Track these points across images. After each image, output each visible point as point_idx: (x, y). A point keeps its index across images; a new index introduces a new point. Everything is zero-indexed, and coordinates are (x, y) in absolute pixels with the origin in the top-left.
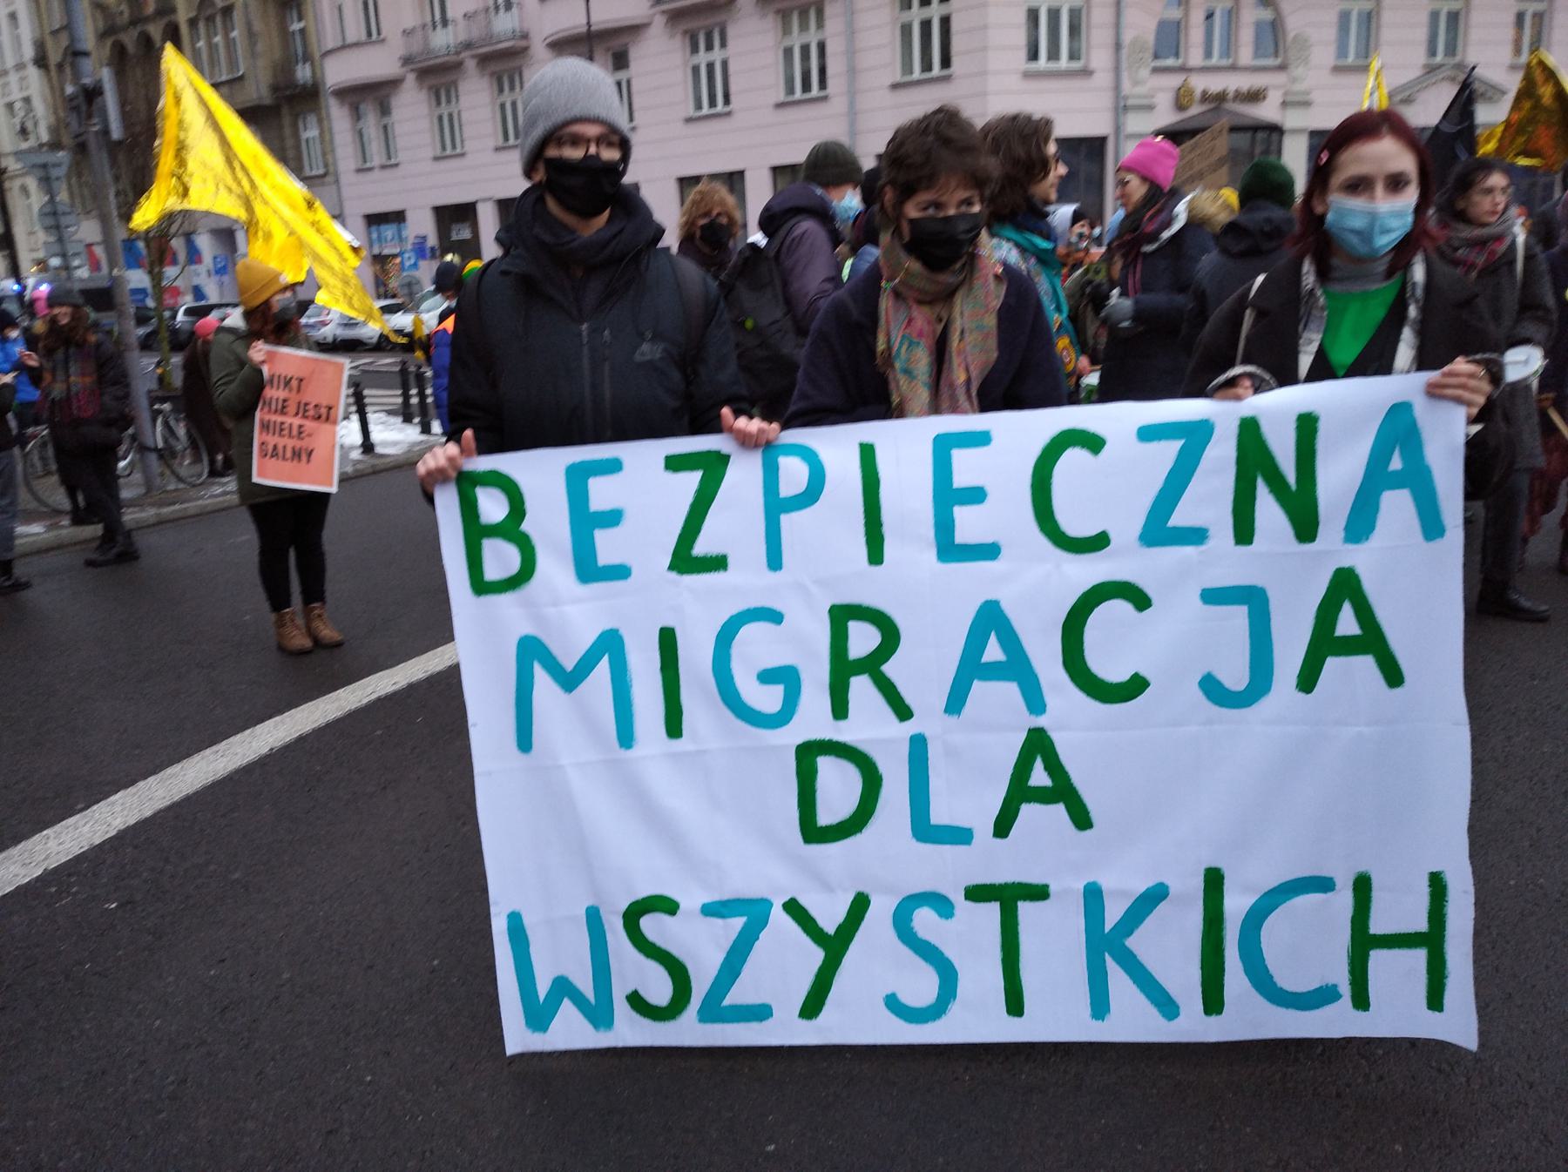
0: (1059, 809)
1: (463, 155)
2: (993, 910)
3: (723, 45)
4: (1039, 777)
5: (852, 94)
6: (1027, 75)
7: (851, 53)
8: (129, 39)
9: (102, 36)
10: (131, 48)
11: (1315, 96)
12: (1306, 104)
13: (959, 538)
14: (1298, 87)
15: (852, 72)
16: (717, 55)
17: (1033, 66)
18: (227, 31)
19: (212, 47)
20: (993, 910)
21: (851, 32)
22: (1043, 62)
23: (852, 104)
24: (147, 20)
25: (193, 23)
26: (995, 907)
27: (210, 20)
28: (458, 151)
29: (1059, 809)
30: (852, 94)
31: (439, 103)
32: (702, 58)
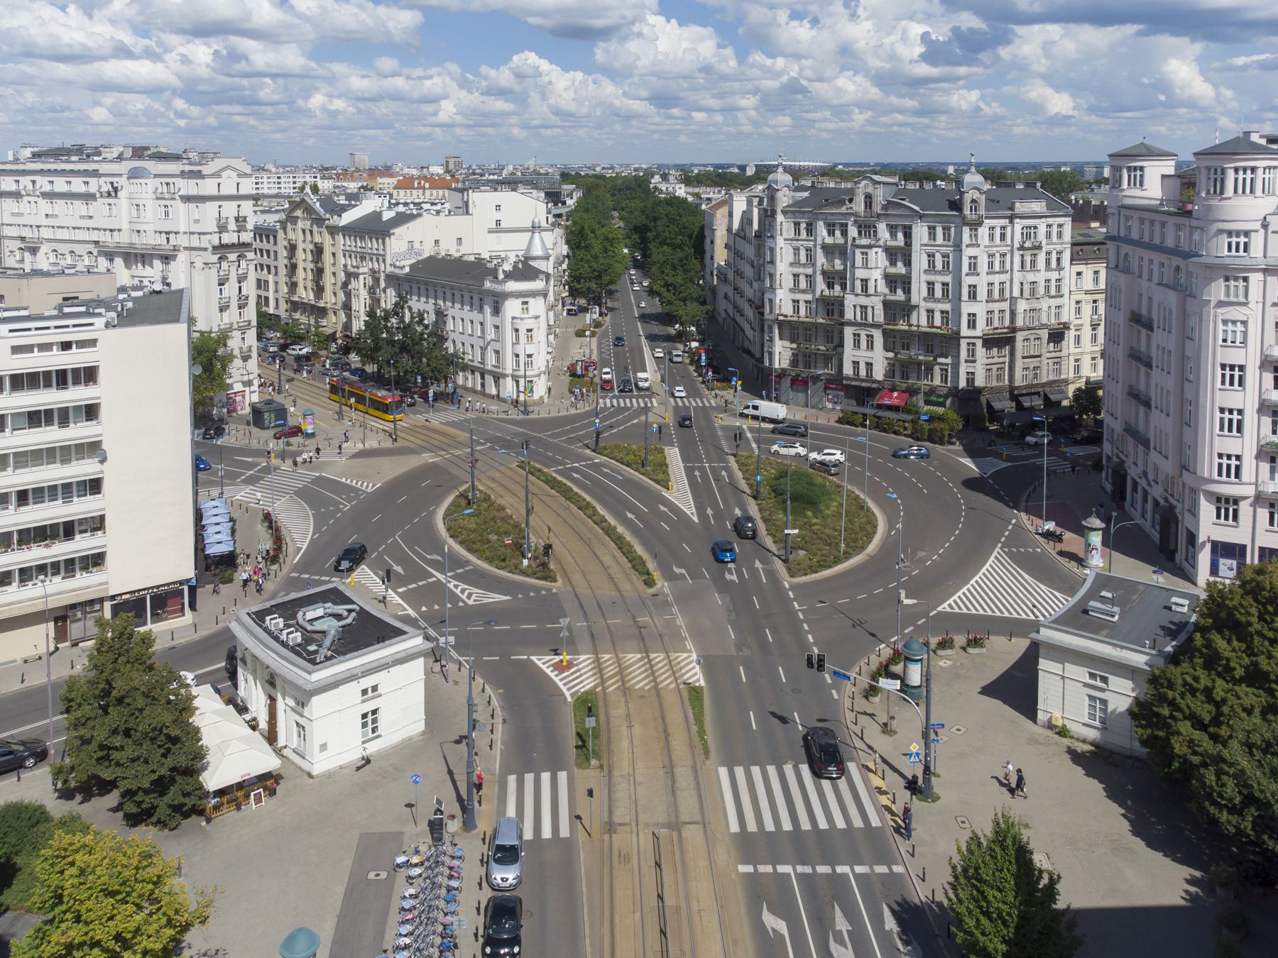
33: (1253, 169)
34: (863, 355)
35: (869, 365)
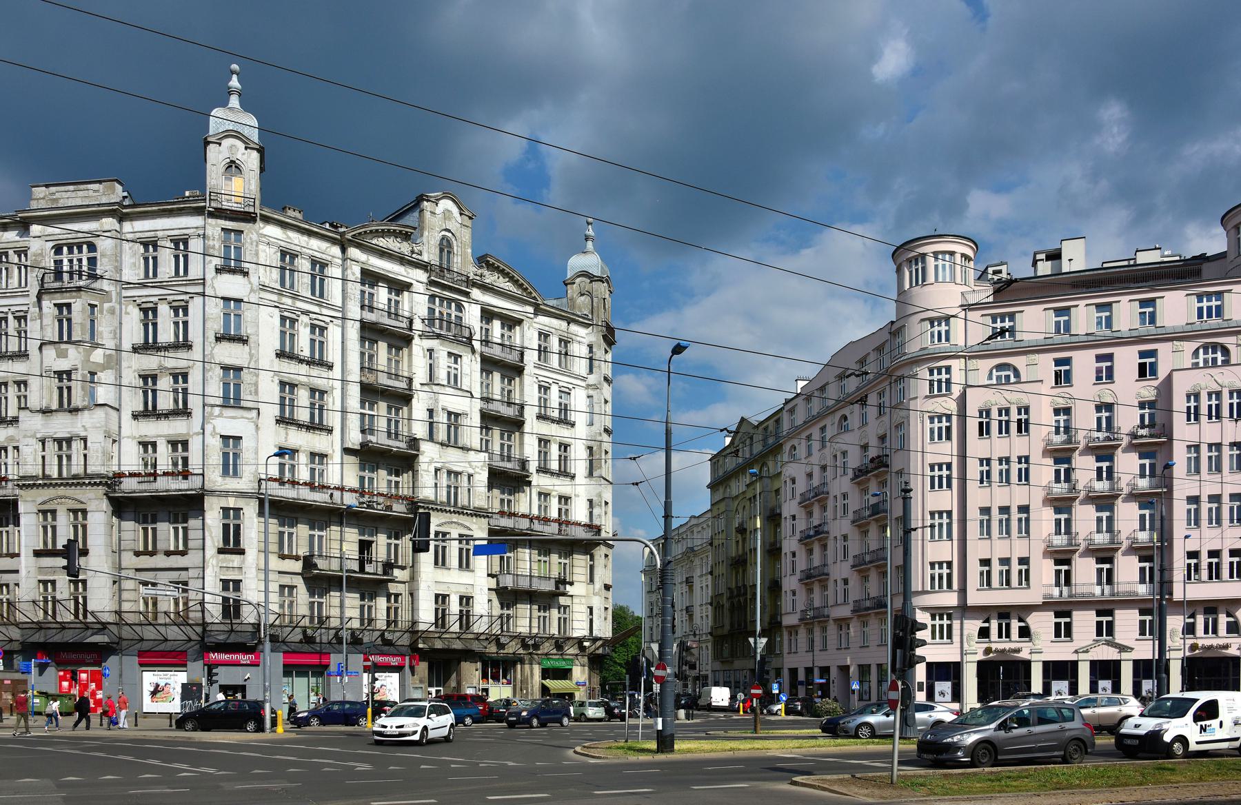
33: (924, 256)
34: (454, 580)
35: (466, 600)
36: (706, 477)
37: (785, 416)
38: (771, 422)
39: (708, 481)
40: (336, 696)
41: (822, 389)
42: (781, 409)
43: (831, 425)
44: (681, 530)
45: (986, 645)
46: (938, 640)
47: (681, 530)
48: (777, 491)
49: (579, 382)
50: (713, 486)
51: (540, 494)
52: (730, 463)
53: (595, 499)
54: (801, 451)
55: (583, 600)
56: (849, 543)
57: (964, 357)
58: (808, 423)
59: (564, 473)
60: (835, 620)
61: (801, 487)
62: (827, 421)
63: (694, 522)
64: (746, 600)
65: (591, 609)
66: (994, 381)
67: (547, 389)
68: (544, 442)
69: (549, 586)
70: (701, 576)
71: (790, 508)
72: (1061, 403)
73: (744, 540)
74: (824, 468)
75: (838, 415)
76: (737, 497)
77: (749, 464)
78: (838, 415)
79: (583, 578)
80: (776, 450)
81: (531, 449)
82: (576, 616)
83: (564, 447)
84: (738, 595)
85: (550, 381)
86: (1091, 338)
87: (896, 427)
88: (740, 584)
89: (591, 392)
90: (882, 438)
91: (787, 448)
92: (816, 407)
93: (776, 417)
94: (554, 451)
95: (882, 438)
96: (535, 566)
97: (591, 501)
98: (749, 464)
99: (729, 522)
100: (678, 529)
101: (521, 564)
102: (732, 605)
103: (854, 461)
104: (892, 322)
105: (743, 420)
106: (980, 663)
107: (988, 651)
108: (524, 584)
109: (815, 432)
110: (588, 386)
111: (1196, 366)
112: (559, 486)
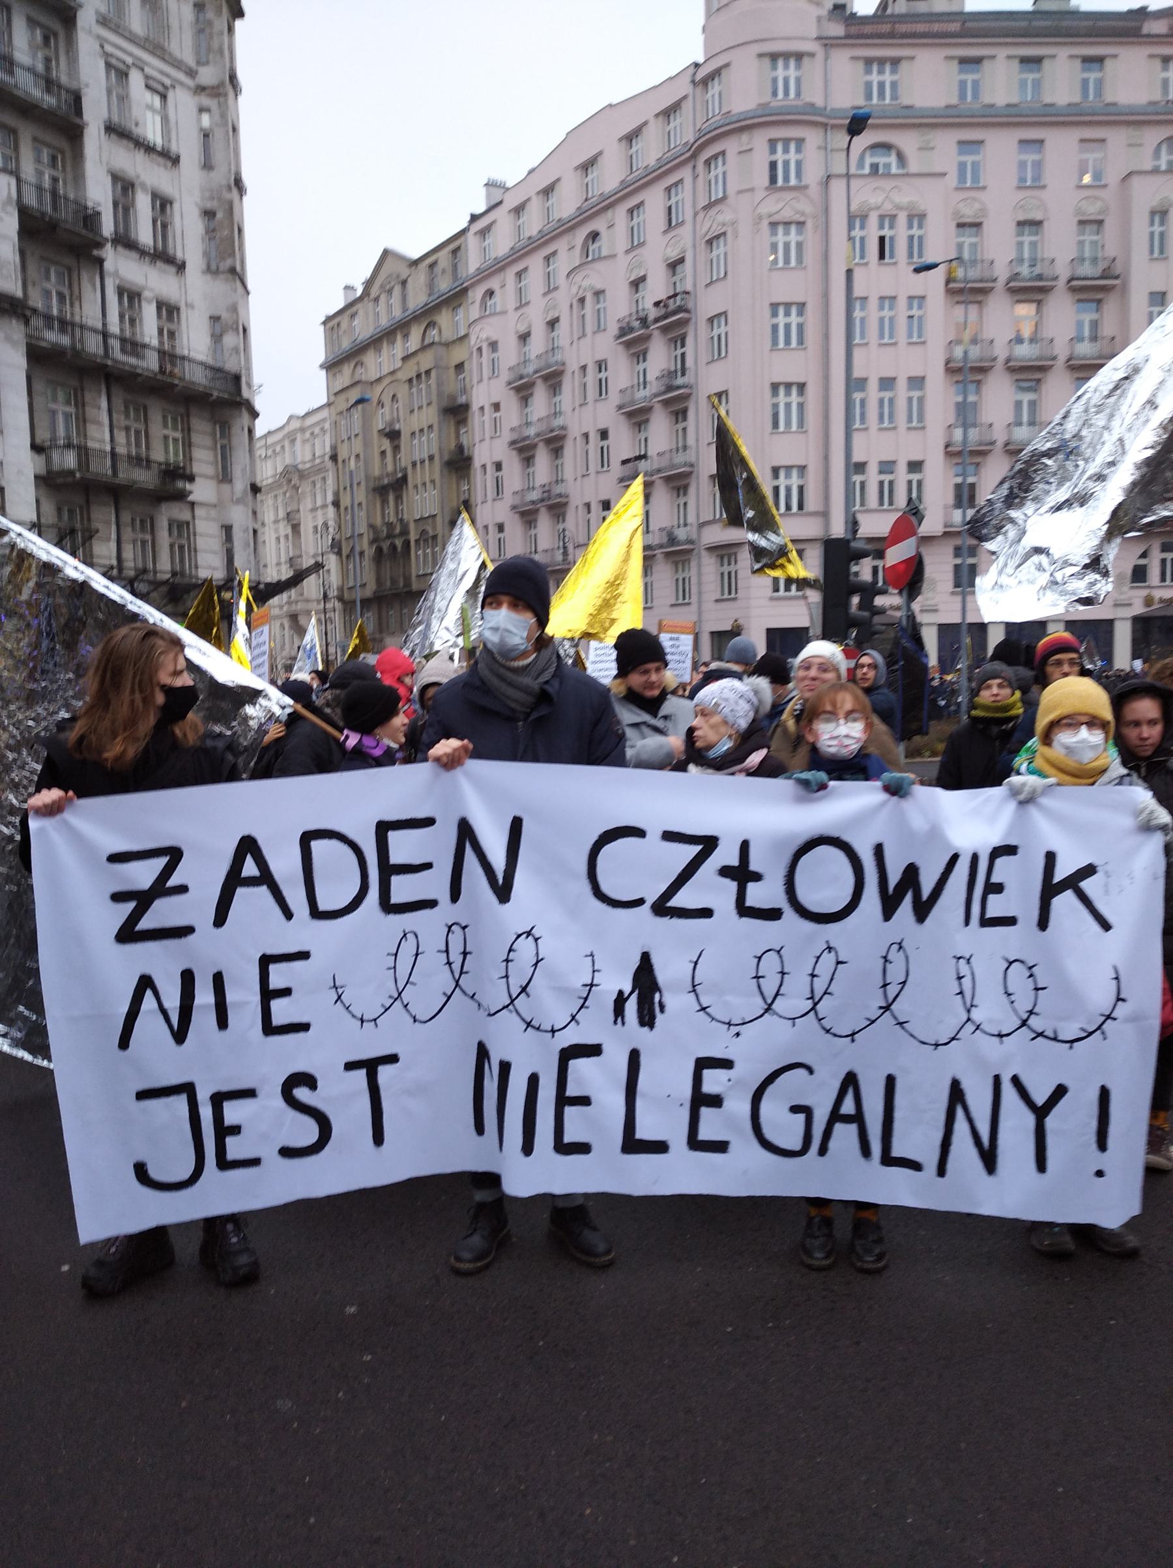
0: (264, 890)
1: (735, 599)
2: (362, 1073)
3: (736, 562)
4: (250, 868)
5: (700, 602)
6: (772, 599)
7: (700, 584)
8: (385, 546)
9: (371, 543)
10: (385, 550)
11: (941, 607)
12: (936, 611)
13: (749, 903)
14: (929, 603)
15: (700, 593)
16: (732, 568)
17: (776, 594)
18: (433, 548)
19: (425, 555)
20: (362, 1073)
21: (699, 574)
22: (782, 592)
23: (700, 608)
24: (395, 536)
25: (417, 541)
26: (364, 1071)
27: (426, 541)
28: (733, 596)
29: (264, 890)
30: (700, 602)
31: (677, 571)
32: (726, 569)
36: (318, 352)
37: (472, 241)
38: (444, 255)
39: (321, 357)
40: (56, 467)
41: (548, 191)
42: (463, 232)
43: (567, 254)
44: (270, 440)
45: (1144, 592)
46: (782, 592)
47: (270, 440)
48: (460, 367)
49: (181, 76)
50: (332, 366)
51: (121, 291)
52: (363, 327)
53: (225, 315)
54: (506, 298)
55: (213, 513)
56: (505, 472)
57: (825, 126)
58: (520, 253)
59: (162, 256)
60: (712, 549)
61: (509, 355)
62: (561, 245)
63: (296, 424)
64: (407, 544)
65: (228, 530)
66: (867, 170)
67: (123, 75)
68: (124, 187)
69: (145, 478)
70: (314, 510)
71: (486, 391)
72: (968, 213)
73: (396, 449)
74: (552, 324)
75: (582, 234)
76: (379, 380)
77: (401, 328)
78: (582, 234)
79: (210, 470)
80: (456, 298)
81: (98, 192)
82: (201, 543)
83: (162, 204)
84: (390, 536)
85: (129, 60)
86: (1013, 111)
87: (710, 242)
88: (392, 519)
89: (206, 101)
90: (674, 266)
91: (477, 294)
92: (533, 223)
93: (454, 245)
94: (143, 205)
95: (674, 266)
96: (121, 438)
97: (215, 319)
98: (401, 328)
99: (366, 422)
100: (265, 436)
101: (92, 430)
102: (379, 550)
103: (619, 306)
104: (697, 65)
105: (386, 253)
106: (1136, 620)
107: (1148, 601)
108: (102, 468)
109: (535, 263)
110: (200, 89)
111: (1156, 171)
112: (155, 281)
